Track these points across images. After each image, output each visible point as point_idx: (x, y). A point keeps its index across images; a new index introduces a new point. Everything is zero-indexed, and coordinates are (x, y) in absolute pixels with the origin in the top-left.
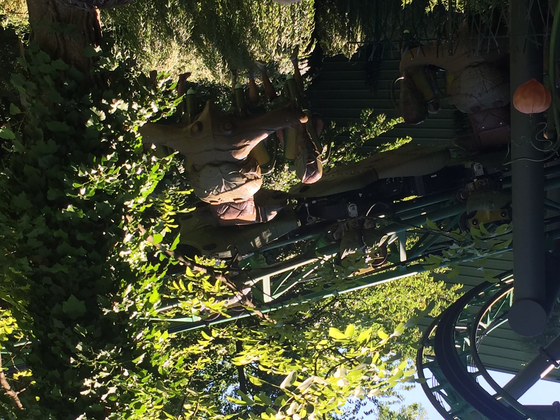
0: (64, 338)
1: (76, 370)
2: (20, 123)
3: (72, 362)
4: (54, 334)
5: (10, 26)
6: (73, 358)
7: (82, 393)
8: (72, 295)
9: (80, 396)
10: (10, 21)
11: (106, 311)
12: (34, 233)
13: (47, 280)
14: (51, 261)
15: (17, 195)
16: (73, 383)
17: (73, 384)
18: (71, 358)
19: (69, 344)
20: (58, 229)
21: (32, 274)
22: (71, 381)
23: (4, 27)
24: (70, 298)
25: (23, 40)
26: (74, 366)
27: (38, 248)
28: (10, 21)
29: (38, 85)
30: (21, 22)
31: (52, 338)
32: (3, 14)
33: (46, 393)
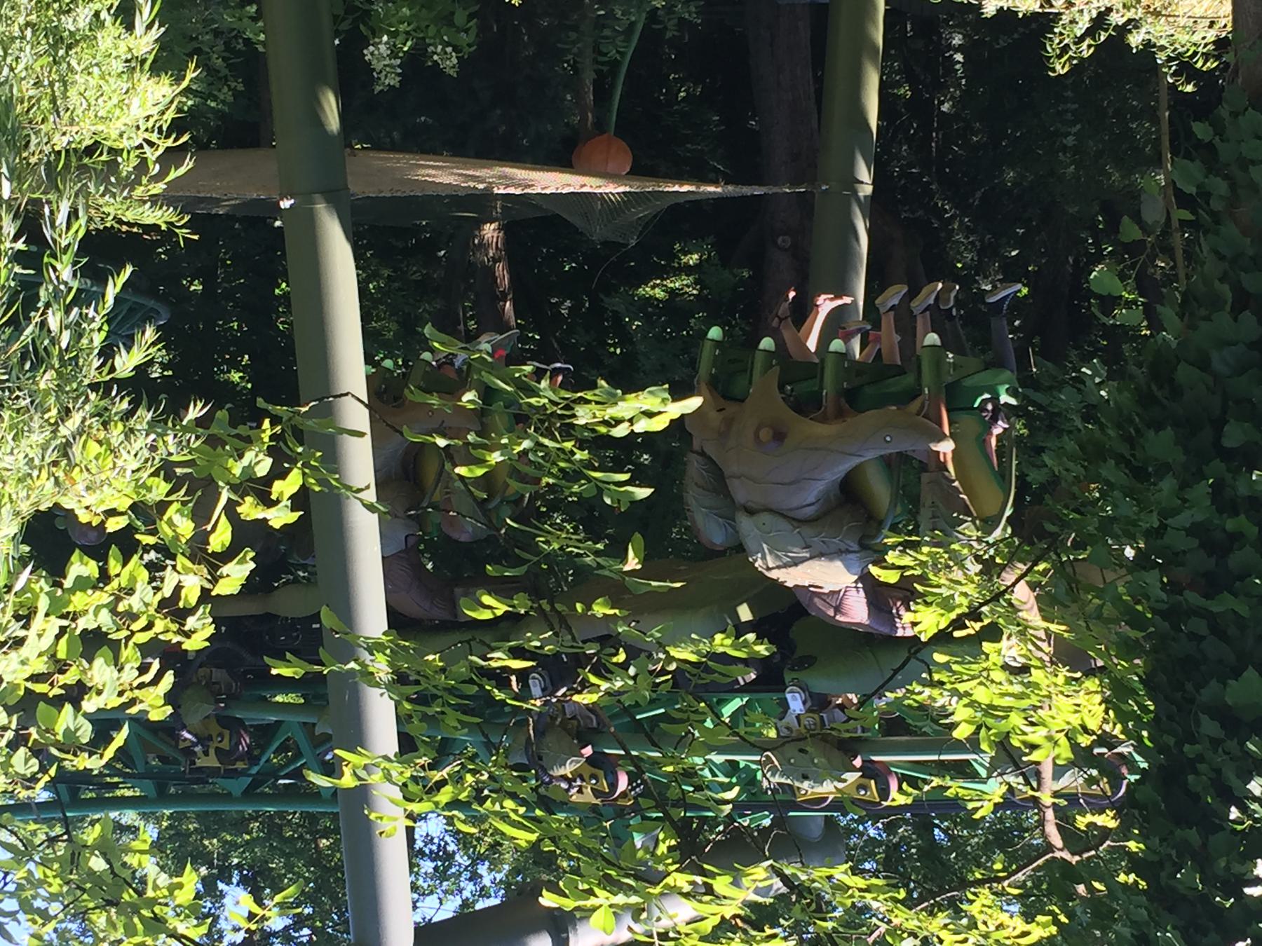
0: (1219, 760)
1: (1239, 837)
2: (1136, 262)
3: (1232, 817)
4: (1197, 746)
5: (1148, 44)
6: (1237, 807)
7: (1248, 891)
8: (1250, 667)
9: (1240, 896)
10: (1149, 33)
11: (229, 406)
12: (1184, 519)
13: (1200, 626)
14: (1213, 585)
15: (1157, 431)
16: (1228, 862)
17: (1227, 868)
18: (1233, 809)
19: (1233, 780)
20: (1237, 515)
21: (1166, 606)
22: (1225, 858)
23: (1133, 45)
24: (1245, 674)
25: (1173, 75)
26: (1235, 826)
27: (1184, 552)
28: (1149, 33)
29: (1233, 186)
30: (1172, 35)
31: (1191, 756)
32: (1134, 16)
33: (1163, 874)
